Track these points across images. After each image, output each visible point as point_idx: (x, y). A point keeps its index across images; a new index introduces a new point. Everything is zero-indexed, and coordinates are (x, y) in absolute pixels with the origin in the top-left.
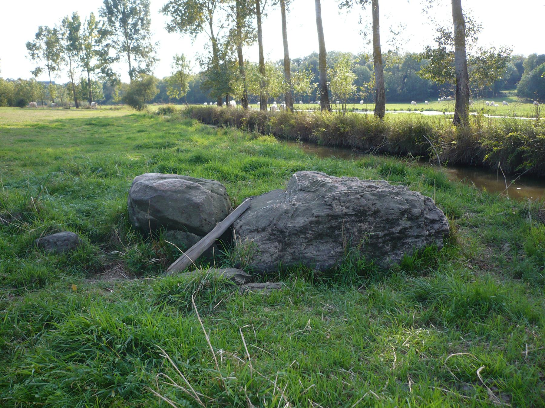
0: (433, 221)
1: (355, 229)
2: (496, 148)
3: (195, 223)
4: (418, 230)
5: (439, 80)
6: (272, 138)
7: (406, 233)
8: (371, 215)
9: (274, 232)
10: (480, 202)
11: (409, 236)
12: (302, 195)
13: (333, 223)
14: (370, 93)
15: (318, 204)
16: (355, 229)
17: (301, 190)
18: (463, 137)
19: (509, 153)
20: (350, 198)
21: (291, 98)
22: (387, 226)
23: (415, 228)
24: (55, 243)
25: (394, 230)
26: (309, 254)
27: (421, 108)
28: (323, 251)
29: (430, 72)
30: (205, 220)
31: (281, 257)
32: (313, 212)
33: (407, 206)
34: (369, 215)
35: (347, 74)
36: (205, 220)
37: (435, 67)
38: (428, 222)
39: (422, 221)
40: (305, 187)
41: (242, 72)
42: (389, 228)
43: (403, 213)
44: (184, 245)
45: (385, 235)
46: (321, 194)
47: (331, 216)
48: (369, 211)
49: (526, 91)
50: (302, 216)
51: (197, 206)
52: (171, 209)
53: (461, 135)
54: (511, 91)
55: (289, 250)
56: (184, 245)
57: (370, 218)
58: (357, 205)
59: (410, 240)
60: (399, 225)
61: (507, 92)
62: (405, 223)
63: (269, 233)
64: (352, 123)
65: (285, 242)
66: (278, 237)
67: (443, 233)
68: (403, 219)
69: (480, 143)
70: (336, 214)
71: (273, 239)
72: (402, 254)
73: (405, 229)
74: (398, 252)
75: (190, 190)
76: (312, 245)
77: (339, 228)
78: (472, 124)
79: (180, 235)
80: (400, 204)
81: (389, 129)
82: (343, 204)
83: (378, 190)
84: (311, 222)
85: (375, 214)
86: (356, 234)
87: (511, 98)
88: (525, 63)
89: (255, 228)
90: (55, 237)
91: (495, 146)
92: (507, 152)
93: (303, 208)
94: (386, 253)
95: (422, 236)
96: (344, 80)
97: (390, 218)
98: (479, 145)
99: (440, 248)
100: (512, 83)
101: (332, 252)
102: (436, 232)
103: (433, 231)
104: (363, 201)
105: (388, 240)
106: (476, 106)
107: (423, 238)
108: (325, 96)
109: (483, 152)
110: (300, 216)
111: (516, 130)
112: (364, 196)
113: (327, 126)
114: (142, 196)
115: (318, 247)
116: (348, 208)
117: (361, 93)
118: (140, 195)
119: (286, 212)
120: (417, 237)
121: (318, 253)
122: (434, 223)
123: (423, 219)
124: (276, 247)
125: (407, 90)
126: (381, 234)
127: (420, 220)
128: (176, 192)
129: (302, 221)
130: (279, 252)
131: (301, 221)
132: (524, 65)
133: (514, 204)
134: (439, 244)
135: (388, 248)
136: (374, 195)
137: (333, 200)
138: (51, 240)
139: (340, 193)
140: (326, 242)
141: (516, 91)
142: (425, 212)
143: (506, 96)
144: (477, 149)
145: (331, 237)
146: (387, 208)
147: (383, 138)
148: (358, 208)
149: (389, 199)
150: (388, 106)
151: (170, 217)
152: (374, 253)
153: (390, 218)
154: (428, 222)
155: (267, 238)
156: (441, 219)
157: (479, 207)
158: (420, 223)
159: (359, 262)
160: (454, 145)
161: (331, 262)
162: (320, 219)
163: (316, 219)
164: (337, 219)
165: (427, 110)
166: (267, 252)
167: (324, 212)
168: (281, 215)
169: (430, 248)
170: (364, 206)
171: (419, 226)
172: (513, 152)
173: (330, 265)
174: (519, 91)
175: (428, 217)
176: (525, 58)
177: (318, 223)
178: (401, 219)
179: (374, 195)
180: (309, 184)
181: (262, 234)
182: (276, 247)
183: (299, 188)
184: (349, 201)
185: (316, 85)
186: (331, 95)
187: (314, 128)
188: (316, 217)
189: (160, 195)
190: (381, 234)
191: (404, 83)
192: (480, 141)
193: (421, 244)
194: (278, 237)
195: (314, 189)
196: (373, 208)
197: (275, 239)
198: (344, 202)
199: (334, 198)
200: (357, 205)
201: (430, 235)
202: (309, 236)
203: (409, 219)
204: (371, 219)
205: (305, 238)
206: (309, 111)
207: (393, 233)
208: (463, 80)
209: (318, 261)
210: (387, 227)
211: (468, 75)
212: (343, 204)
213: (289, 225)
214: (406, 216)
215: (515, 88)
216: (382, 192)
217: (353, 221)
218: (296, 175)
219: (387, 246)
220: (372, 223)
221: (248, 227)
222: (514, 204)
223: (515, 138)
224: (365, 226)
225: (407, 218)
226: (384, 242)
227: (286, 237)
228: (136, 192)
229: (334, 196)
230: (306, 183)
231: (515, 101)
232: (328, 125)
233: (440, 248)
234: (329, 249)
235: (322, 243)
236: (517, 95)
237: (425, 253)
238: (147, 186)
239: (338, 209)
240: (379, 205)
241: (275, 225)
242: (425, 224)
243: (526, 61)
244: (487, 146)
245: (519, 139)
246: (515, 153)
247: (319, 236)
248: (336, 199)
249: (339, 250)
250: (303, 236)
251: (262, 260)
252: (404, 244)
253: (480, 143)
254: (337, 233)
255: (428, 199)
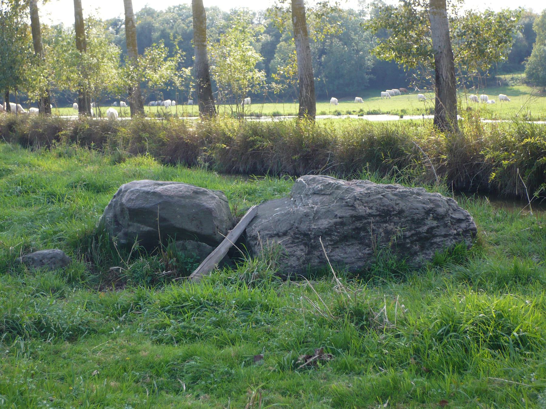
0: (460, 221)
1: (381, 230)
2: (506, 162)
3: (207, 230)
4: (445, 229)
5: (407, 62)
6: (149, 159)
7: (434, 232)
8: (396, 215)
9: (297, 236)
10: (497, 220)
11: (437, 236)
12: (317, 198)
13: (358, 224)
14: (290, 85)
15: (339, 206)
16: (381, 230)
17: (314, 193)
18: (456, 148)
19: (526, 167)
20: (372, 198)
21: (140, 96)
22: (413, 226)
23: (442, 228)
24: (41, 261)
25: (420, 229)
26: (336, 257)
27: (358, 110)
28: (350, 253)
29: (393, 49)
30: (217, 228)
31: (307, 261)
32: (336, 213)
33: (431, 206)
34: (393, 215)
35: (249, 53)
36: (217, 228)
37: (401, 41)
38: (455, 221)
39: (448, 220)
40: (319, 190)
41: (37, 47)
42: (415, 228)
43: (428, 212)
44: (195, 255)
45: (412, 235)
46: (339, 196)
47: (355, 217)
48: (394, 211)
49: (541, 74)
50: (325, 218)
51: (209, 212)
52: (179, 216)
53: (453, 145)
54: (515, 76)
55: (316, 253)
56: (195, 255)
57: (395, 218)
58: (380, 205)
59: (438, 240)
60: (425, 224)
61: (508, 77)
62: (431, 222)
63: (291, 236)
64: (273, 134)
65: (311, 244)
66: (303, 240)
67: (471, 232)
68: (429, 218)
69: (483, 156)
70: (360, 214)
71: (297, 242)
72: (431, 254)
73: (432, 228)
74: (428, 252)
75: (198, 195)
76: (338, 247)
77: (364, 229)
78: (467, 129)
79: (190, 244)
80: (424, 203)
81: (335, 142)
82: (366, 204)
83: (398, 190)
84: (336, 224)
85: (400, 214)
86: (383, 235)
87: (516, 88)
88: (537, 25)
89: (275, 232)
90: (39, 254)
91: (504, 159)
92: (524, 166)
93: (324, 210)
94: (416, 253)
95: (450, 235)
96: (236, 59)
97: (416, 217)
98: (481, 159)
99: (469, 247)
100: (516, 61)
101: (360, 254)
102: (464, 231)
103: (459, 230)
104: (386, 201)
105: (416, 241)
106: (466, 100)
107: (451, 237)
108: (205, 93)
109: (488, 170)
110: (321, 219)
111: (533, 135)
112: (386, 196)
113: (228, 140)
114: (143, 204)
115: (345, 250)
116: (371, 208)
117: (274, 85)
118: (140, 202)
119: (307, 215)
120: (445, 236)
121: (346, 256)
122: (460, 222)
123: (450, 219)
124: (302, 250)
125: (326, 77)
126: (408, 234)
127: (446, 219)
128: (183, 197)
129: (326, 222)
130: (305, 254)
131: (324, 223)
132: (535, 28)
133: (539, 219)
134: (468, 243)
135: (417, 248)
136: (395, 195)
137: (355, 200)
138: (36, 258)
139: (361, 194)
140: (352, 244)
141: (524, 75)
142: (450, 212)
143: (507, 85)
144: (478, 165)
145: (356, 239)
146: (410, 208)
147: (327, 155)
148: (382, 208)
149: (411, 198)
150: (320, 107)
151: (178, 225)
152: (403, 254)
153: (416, 217)
154: (455, 221)
155: (290, 241)
156: (467, 219)
157: (497, 226)
158: (446, 222)
159: (390, 262)
160: (444, 160)
161: (360, 264)
162: (344, 220)
163: (340, 220)
164: (361, 220)
165: (369, 113)
166: (294, 256)
167: (347, 213)
168: (302, 218)
169: (460, 246)
170: (388, 206)
171: (446, 225)
172: (530, 166)
173: (359, 267)
174: (530, 75)
175: (454, 216)
176: (537, 16)
177: (342, 224)
178: (427, 219)
179: (395, 195)
180: (322, 187)
181: (286, 238)
182: (302, 250)
183: (311, 191)
184: (372, 201)
185: (187, 71)
186: (217, 89)
187: (202, 144)
188: (340, 218)
189: (167, 201)
190: (408, 234)
191: (320, 64)
192: (482, 153)
193: (450, 243)
194: (303, 240)
195: (328, 192)
196: (397, 208)
197: (300, 242)
198: (367, 203)
199: (355, 199)
200: (380, 205)
201: (458, 234)
202: (334, 238)
203: (435, 218)
204: (396, 219)
205: (331, 241)
206: (188, 117)
207: (419, 233)
208: (444, 62)
209: (347, 263)
210: (413, 227)
211: (452, 54)
212: (366, 204)
213: (313, 227)
214: (431, 215)
215: (521, 69)
216: (402, 192)
217: (377, 222)
218: (302, 180)
219: (416, 246)
220: (398, 223)
221: (267, 232)
222: (539, 219)
223: (533, 146)
224: (390, 227)
225: (433, 217)
226: (412, 242)
227: (311, 239)
228: (133, 200)
229: (355, 197)
230: (320, 186)
231: (525, 93)
232: (229, 137)
233: (469, 247)
234: (355, 252)
235: (348, 245)
236: (527, 83)
237: (455, 252)
238: (148, 193)
239: (362, 210)
240: (402, 205)
241: (297, 228)
242: (452, 224)
243: (537, 20)
244: (493, 159)
245: (538, 148)
246: (534, 169)
247: (345, 239)
248: (358, 199)
249: (367, 252)
250: (329, 238)
251: (289, 264)
252: (432, 244)
253: (483, 156)
254: (363, 234)
255: (450, 200)
